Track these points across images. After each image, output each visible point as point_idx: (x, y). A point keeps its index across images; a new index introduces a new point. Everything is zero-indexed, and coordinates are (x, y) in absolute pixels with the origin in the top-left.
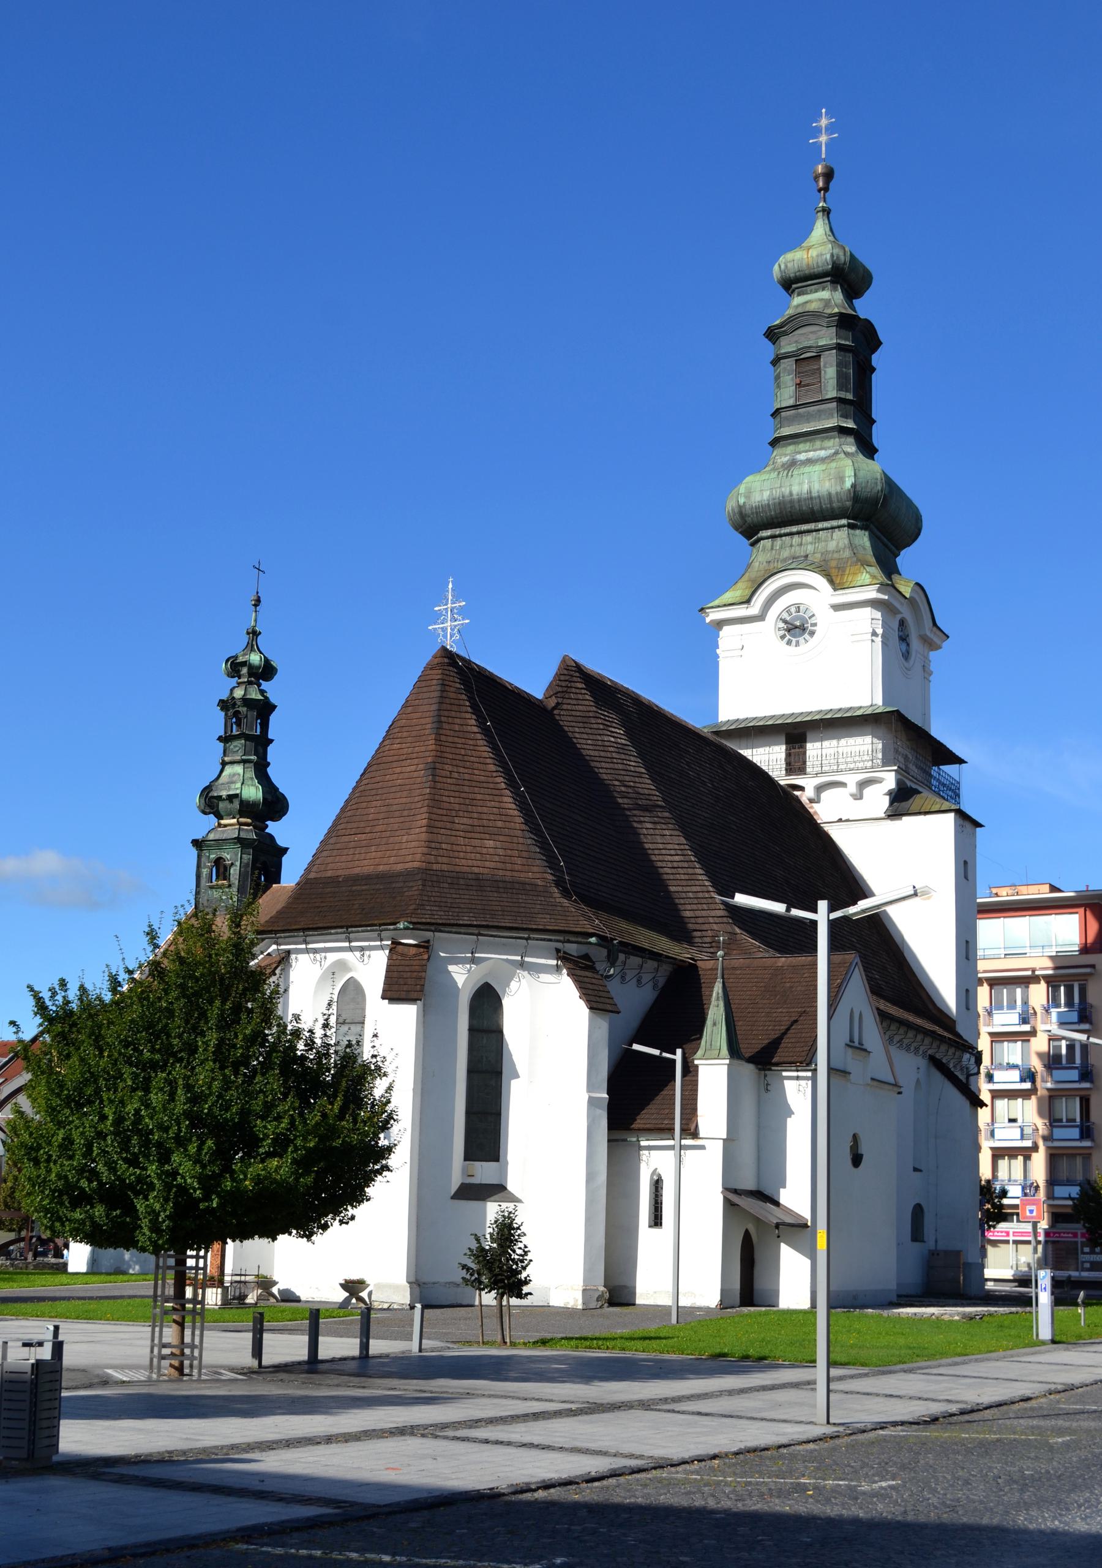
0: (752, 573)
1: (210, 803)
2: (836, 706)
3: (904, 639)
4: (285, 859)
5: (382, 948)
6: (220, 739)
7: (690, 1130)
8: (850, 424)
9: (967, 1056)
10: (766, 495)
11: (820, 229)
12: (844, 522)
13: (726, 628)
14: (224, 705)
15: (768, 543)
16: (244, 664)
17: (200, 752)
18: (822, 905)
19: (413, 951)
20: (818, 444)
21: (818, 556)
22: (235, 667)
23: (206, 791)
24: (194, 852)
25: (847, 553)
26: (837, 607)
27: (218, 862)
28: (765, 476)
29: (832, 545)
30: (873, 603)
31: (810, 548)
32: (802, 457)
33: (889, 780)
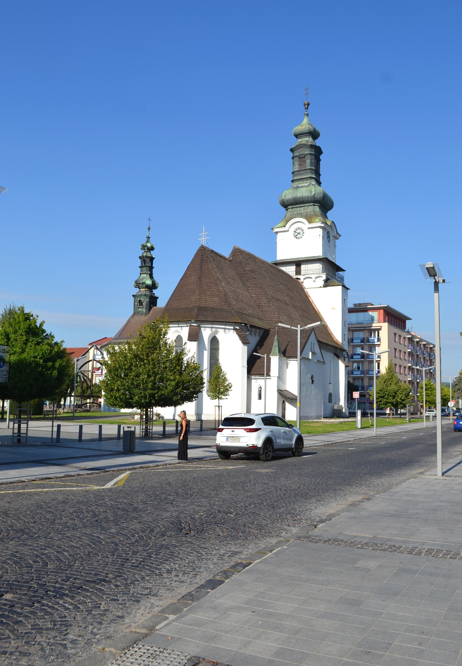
0: (286, 218)
1: (138, 284)
2: (309, 256)
3: (328, 237)
4: (158, 300)
5: (187, 326)
6: (140, 267)
7: (268, 375)
8: (314, 176)
9: (344, 353)
10: (290, 196)
11: (306, 120)
12: (312, 204)
13: (279, 234)
14: (140, 258)
15: (291, 210)
16: (146, 246)
17: (134, 271)
18: (299, 326)
19: (195, 328)
20: (305, 181)
21: (305, 213)
22: (144, 247)
23: (136, 282)
24: (133, 298)
25: (313, 213)
26: (309, 228)
27: (140, 301)
28: (290, 191)
29: (308, 211)
30: (320, 227)
31: (302, 211)
32: (300, 185)
33: (324, 277)
